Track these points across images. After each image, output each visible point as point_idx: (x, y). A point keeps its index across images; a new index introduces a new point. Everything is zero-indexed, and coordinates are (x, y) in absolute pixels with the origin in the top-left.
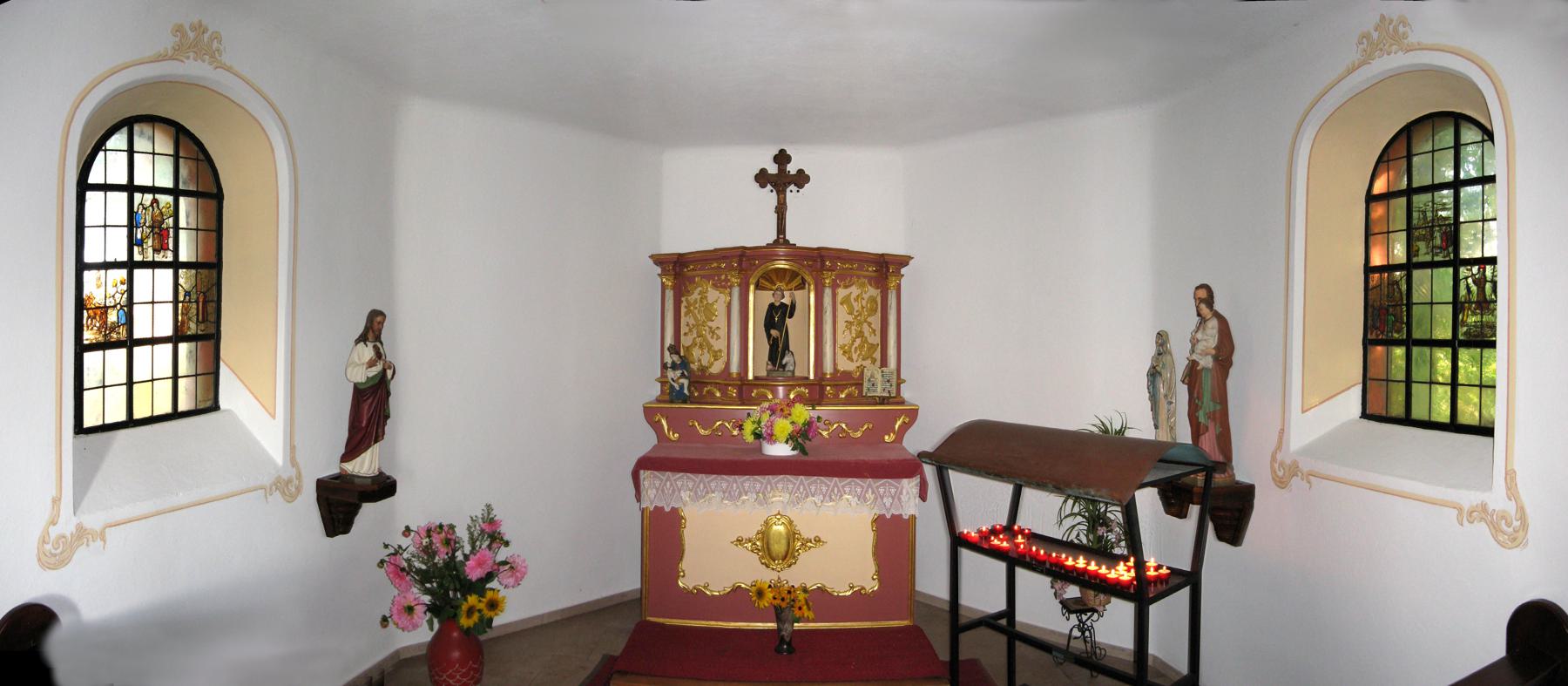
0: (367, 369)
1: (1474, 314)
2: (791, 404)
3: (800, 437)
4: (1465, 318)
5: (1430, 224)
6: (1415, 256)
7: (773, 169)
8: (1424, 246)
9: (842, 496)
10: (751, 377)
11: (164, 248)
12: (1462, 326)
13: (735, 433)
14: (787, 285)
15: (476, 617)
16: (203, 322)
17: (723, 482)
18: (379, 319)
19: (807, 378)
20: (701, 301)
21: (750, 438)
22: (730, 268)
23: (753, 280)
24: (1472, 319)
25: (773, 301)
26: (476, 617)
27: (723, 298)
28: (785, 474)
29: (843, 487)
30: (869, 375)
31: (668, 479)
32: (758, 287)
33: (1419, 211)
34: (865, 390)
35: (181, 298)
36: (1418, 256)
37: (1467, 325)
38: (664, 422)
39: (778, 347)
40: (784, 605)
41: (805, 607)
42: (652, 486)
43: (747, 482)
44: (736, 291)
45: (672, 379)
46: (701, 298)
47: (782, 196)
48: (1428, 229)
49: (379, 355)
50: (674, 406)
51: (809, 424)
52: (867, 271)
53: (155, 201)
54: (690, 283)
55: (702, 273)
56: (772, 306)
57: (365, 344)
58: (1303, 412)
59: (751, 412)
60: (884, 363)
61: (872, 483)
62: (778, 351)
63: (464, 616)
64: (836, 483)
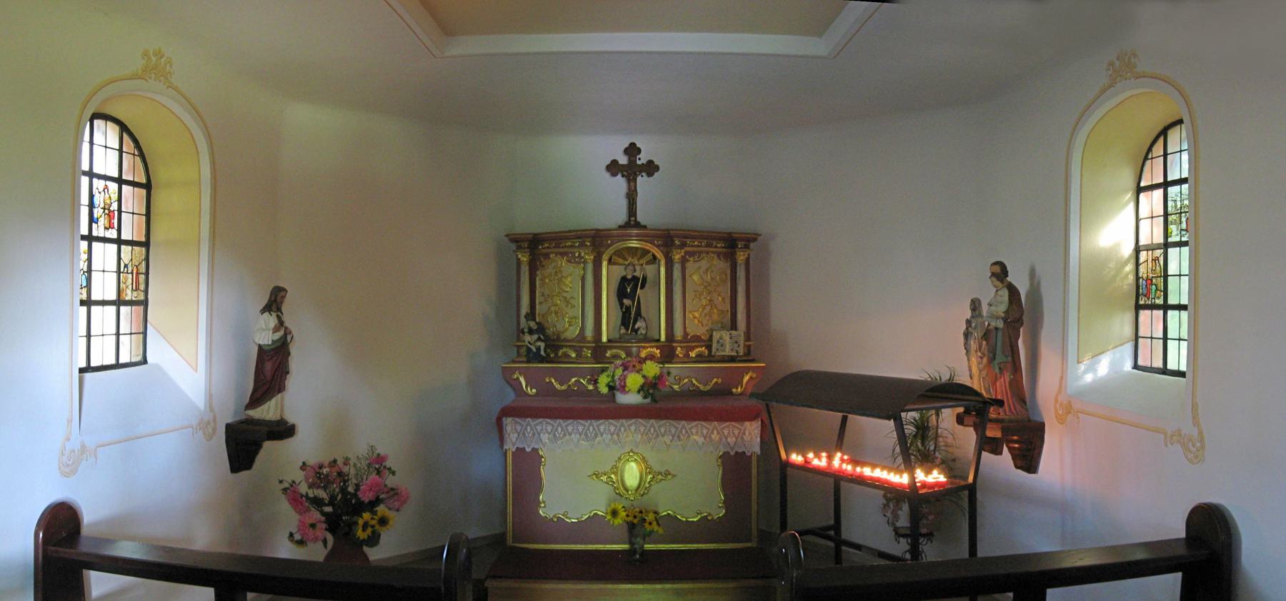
0: (273, 333)
2: (643, 361)
3: (649, 387)
7: (623, 160)
8: (1175, 229)
9: (689, 436)
10: (604, 339)
11: (111, 226)
13: (591, 387)
14: (638, 261)
15: (369, 530)
16: (136, 290)
17: (581, 425)
18: (282, 294)
19: (658, 340)
20: (556, 274)
21: (604, 390)
22: (582, 245)
23: (605, 258)
25: (625, 274)
26: (369, 530)
27: (578, 271)
28: (699, 420)
29: (691, 429)
30: (718, 337)
31: (528, 424)
32: (610, 261)
34: (714, 350)
35: (122, 270)
38: (522, 380)
39: (630, 314)
40: (636, 521)
41: (655, 523)
42: (731, 434)
43: (603, 425)
44: (590, 267)
45: (529, 343)
46: (556, 272)
47: (632, 184)
48: (1178, 215)
49: (281, 323)
50: (531, 365)
51: (660, 378)
52: (716, 247)
53: (106, 187)
54: (545, 259)
55: (556, 250)
56: (624, 279)
57: (270, 313)
59: (671, 371)
60: (734, 326)
61: (654, 423)
62: (629, 318)
63: (361, 529)
64: (560, 424)
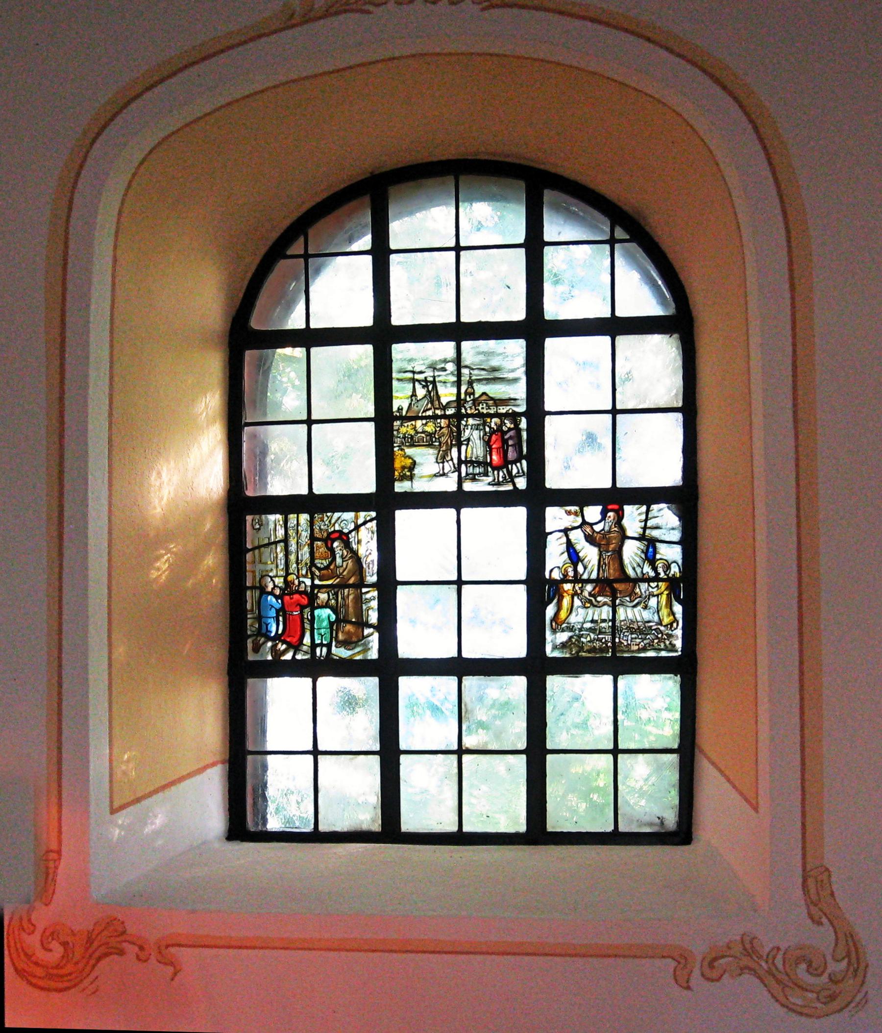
1: (590, 603)
4: (563, 614)
5: (450, 412)
6: (402, 478)
12: (554, 631)
24: (580, 616)
33: (414, 381)
36: (411, 478)
37: (571, 629)
58: (113, 811)
